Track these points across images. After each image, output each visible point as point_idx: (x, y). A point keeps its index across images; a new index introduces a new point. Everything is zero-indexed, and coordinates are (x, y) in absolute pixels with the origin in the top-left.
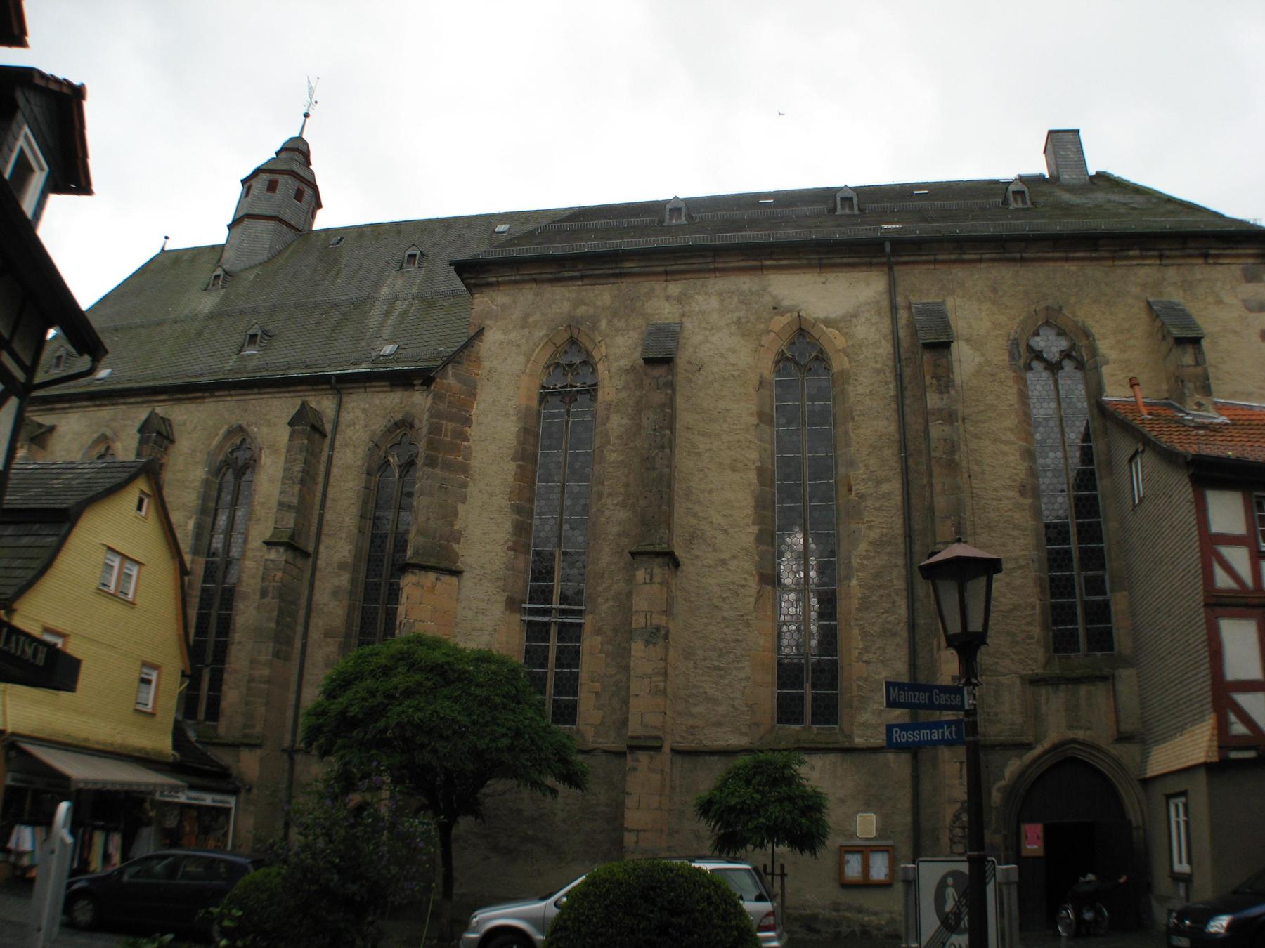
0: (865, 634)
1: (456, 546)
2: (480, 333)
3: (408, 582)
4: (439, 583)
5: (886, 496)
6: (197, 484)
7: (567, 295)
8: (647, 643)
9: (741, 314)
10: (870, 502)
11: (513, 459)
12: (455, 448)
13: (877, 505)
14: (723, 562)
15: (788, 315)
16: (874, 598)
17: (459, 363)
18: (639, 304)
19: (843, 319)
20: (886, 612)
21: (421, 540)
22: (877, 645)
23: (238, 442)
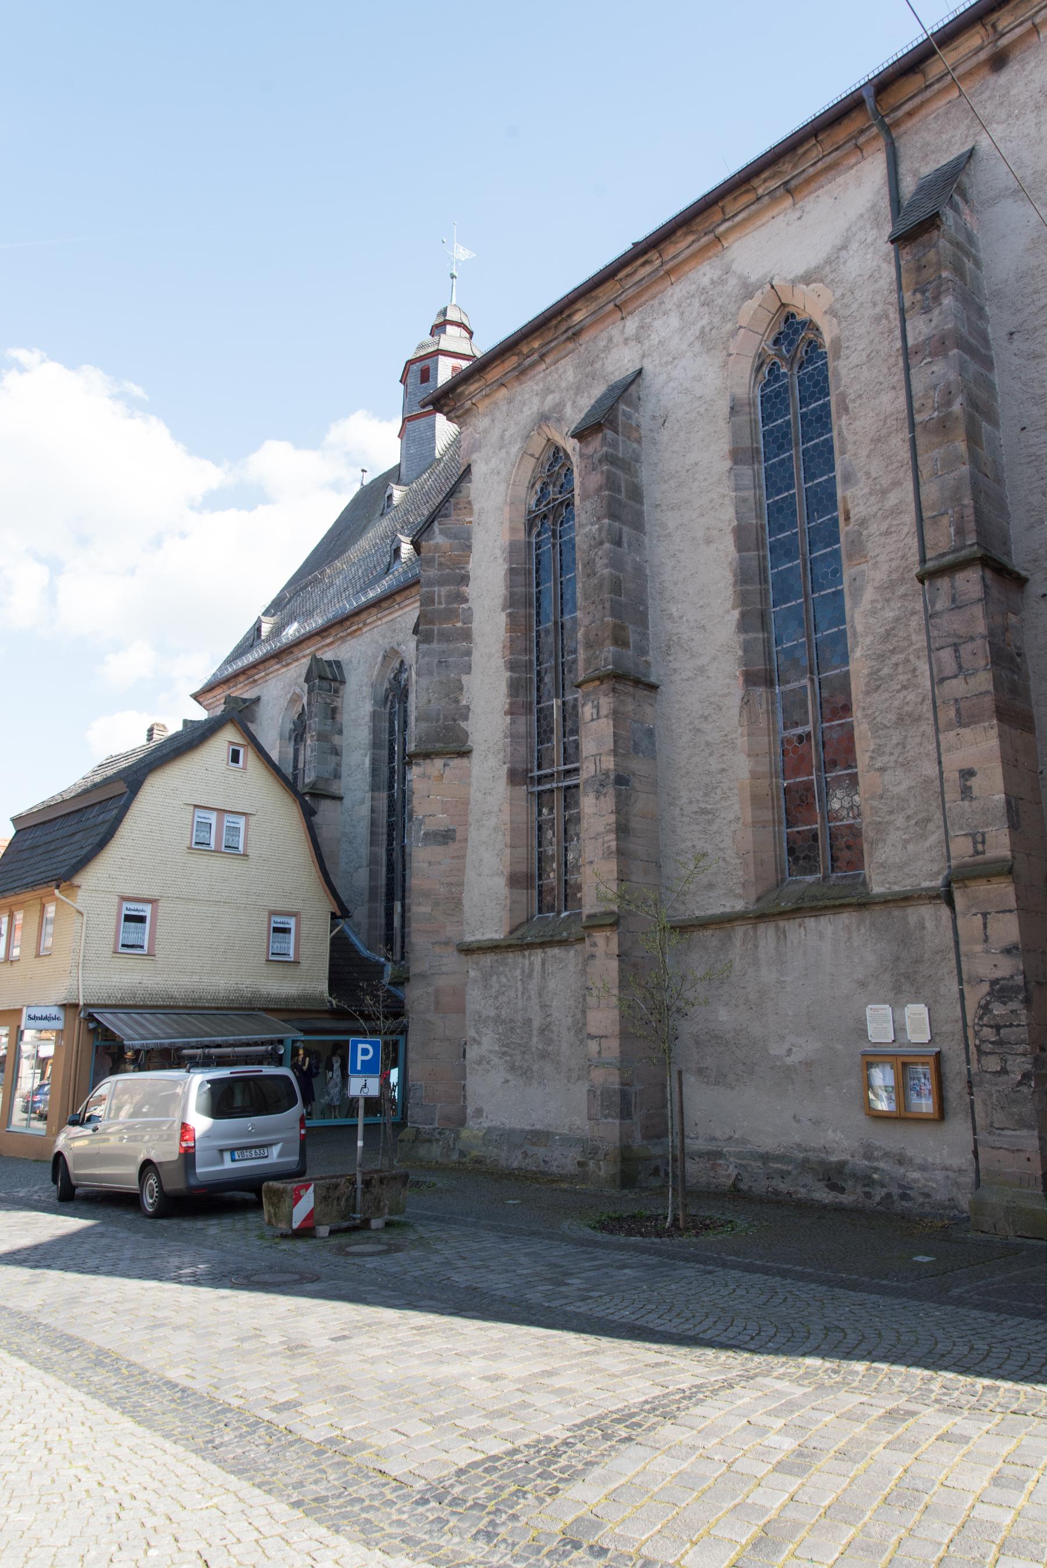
0: (876, 728)
1: (463, 724)
2: (468, 470)
3: (414, 773)
4: (448, 771)
5: (896, 511)
6: (367, 719)
7: (536, 388)
8: (598, 795)
9: (704, 322)
10: (873, 528)
11: (503, 610)
12: (451, 614)
13: (884, 527)
14: (702, 670)
15: (758, 293)
16: (886, 671)
17: (446, 516)
18: (598, 365)
19: (828, 261)
20: (905, 687)
21: (424, 725)
22: (894, 742)
23: (397, 665)
